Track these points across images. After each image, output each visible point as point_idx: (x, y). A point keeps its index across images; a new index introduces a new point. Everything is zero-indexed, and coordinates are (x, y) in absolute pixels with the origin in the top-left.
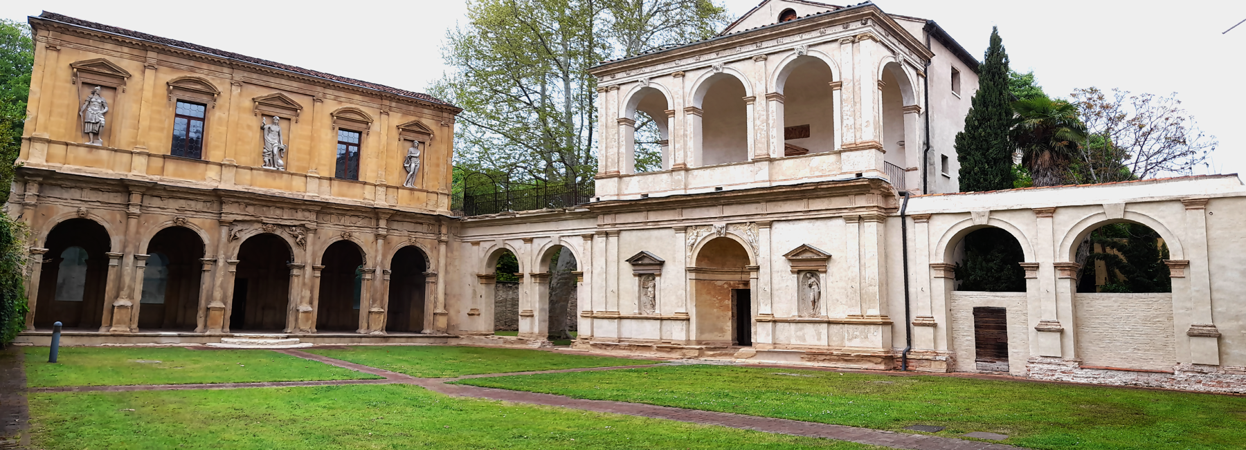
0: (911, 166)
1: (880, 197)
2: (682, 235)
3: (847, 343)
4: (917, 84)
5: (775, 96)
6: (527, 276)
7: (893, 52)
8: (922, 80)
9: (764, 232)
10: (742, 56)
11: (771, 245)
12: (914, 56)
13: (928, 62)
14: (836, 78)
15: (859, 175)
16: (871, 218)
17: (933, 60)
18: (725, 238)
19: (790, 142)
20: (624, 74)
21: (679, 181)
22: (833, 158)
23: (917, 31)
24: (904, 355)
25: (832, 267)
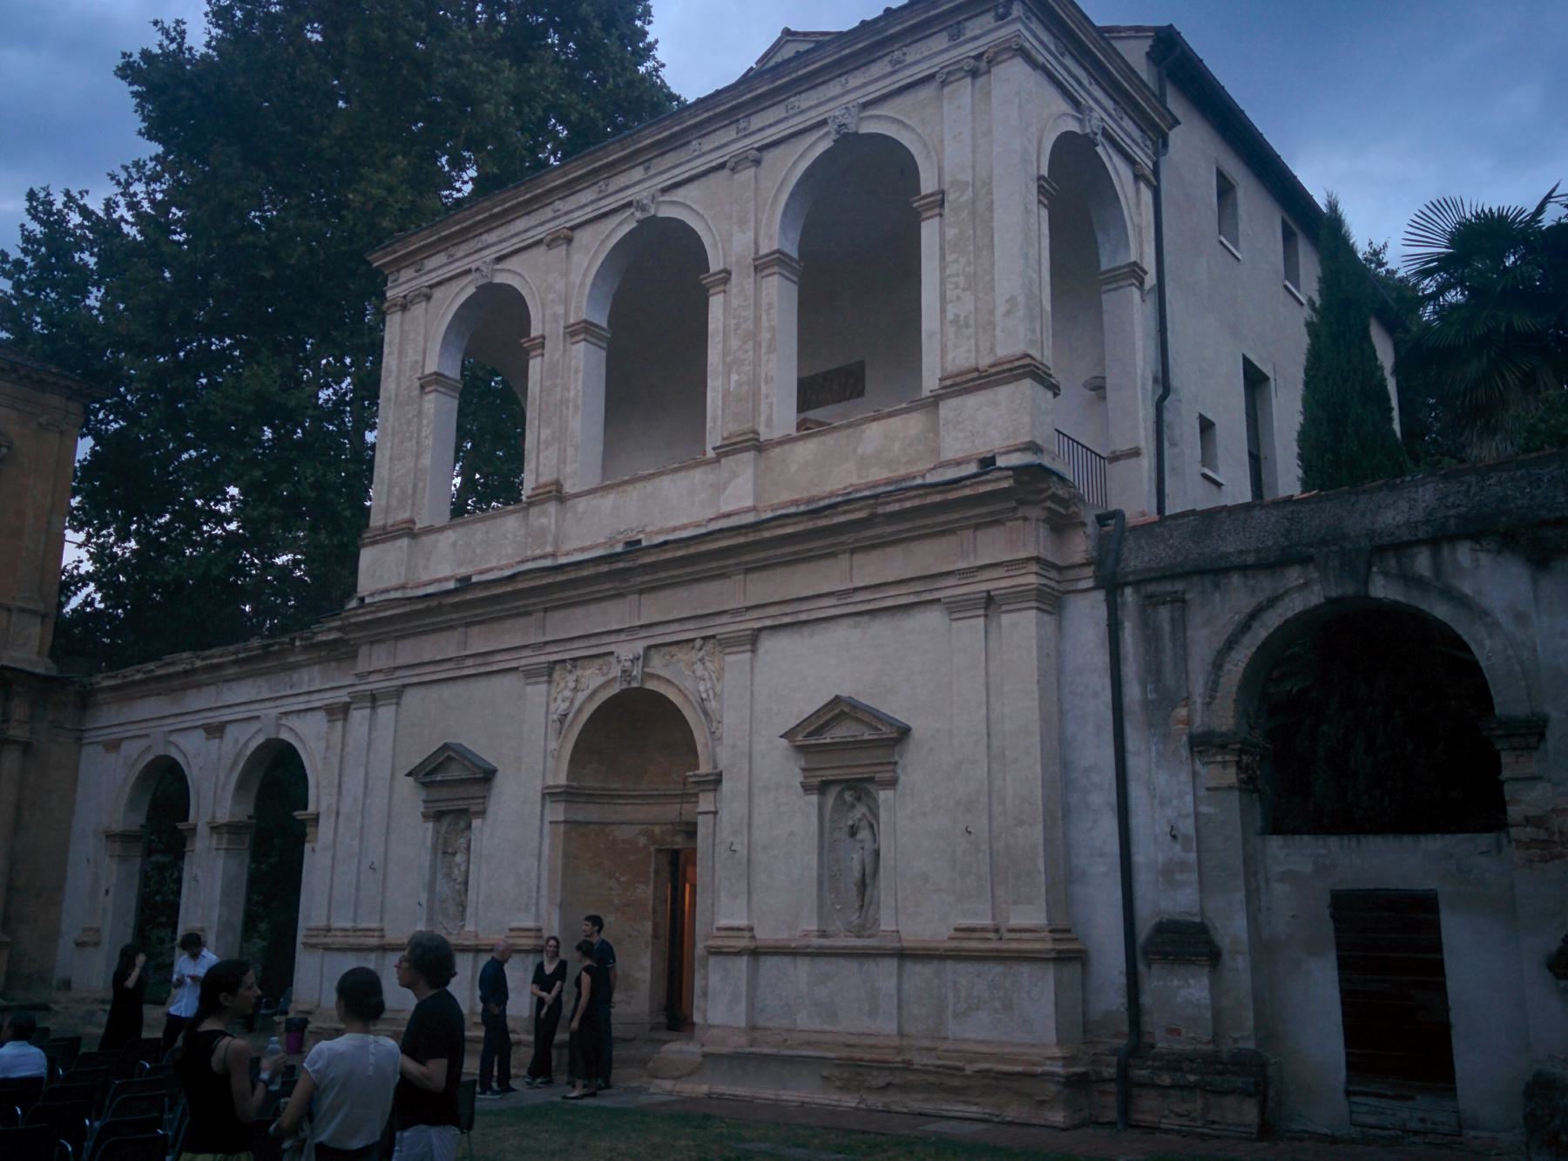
0: (1122, 446)
1: (1044, 530)
2: (537, 691)
3: (954, 1029)
4: (1135, 204)
5: (779, 259)
6: (203, 830)
7: (1076, 104)
8: (1147, 195)
9: (738, 660)
10: (699, 165)
11: (754, 699)
12: (1128, 124)
13: (1160, 143)
14: (927, 185)
15: (987, 463)
16: (1016, 597)
17: (1175, 136)
18: (641, 691)
19: (803, 415)
20: (441, 259)
21: (543, 531)
22: (913, 424)
23: (1135, 54)
24: (1123, 1068)
25: (914, 768)
